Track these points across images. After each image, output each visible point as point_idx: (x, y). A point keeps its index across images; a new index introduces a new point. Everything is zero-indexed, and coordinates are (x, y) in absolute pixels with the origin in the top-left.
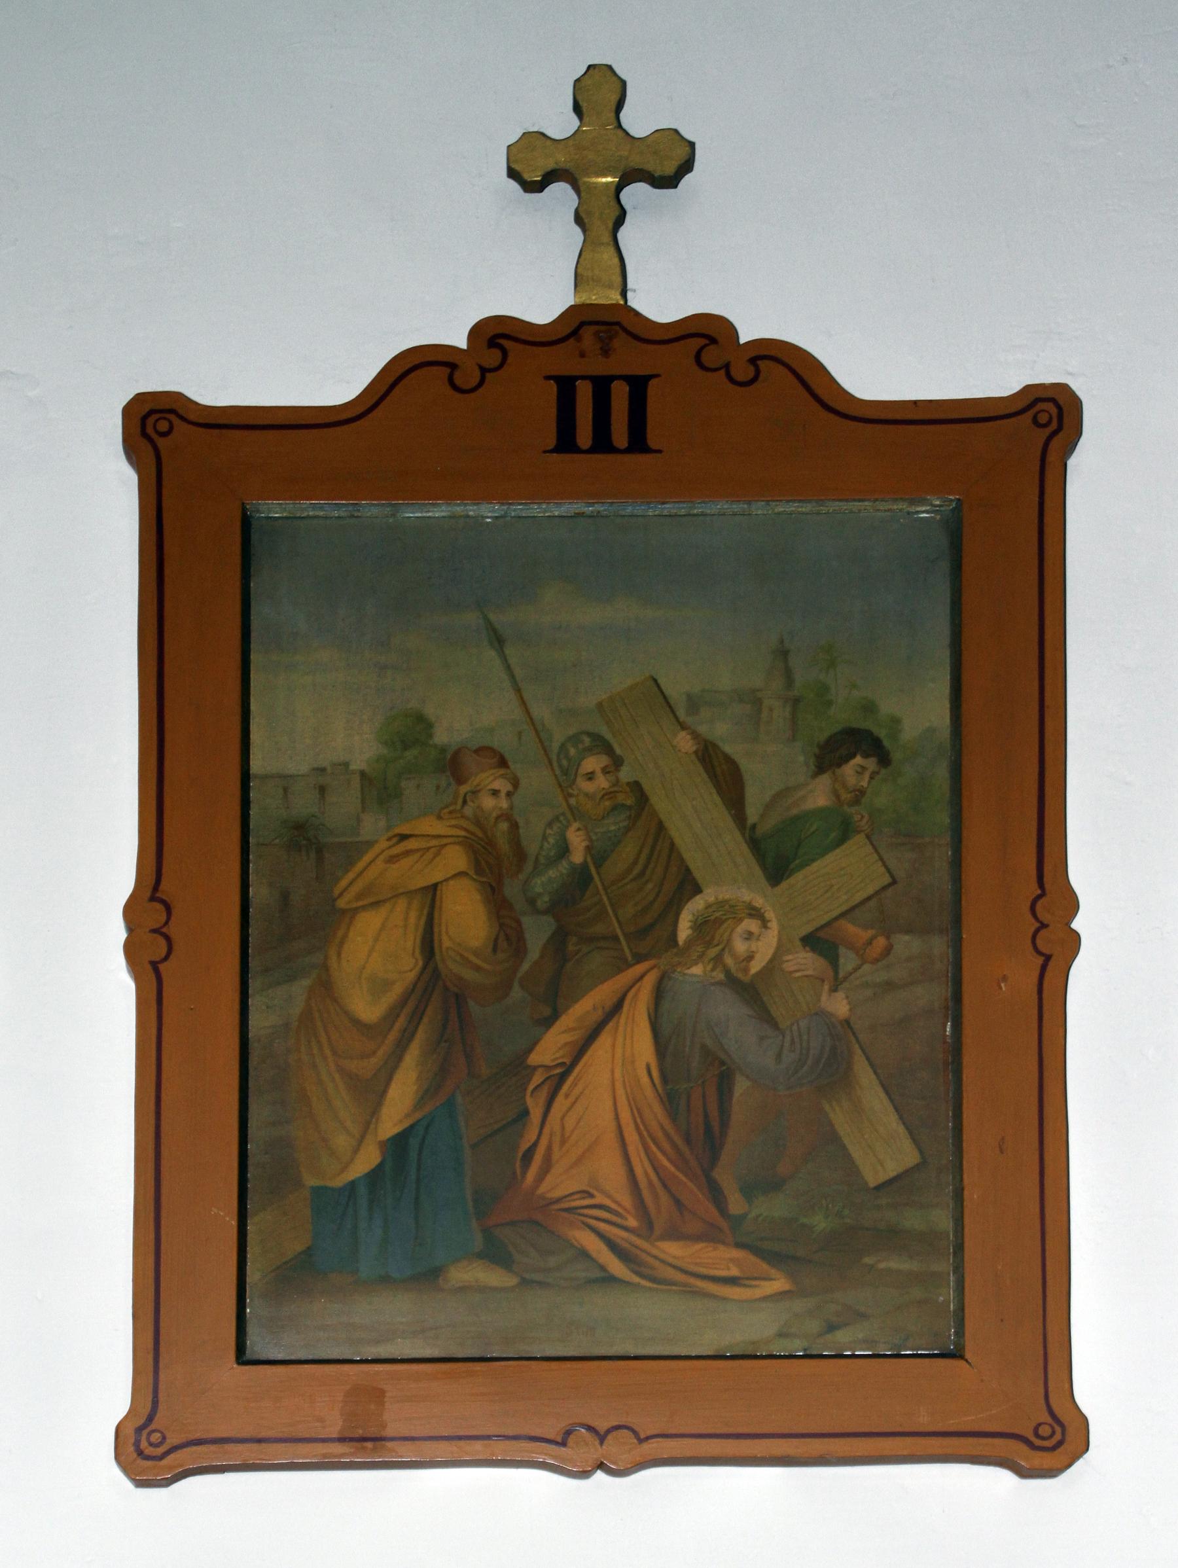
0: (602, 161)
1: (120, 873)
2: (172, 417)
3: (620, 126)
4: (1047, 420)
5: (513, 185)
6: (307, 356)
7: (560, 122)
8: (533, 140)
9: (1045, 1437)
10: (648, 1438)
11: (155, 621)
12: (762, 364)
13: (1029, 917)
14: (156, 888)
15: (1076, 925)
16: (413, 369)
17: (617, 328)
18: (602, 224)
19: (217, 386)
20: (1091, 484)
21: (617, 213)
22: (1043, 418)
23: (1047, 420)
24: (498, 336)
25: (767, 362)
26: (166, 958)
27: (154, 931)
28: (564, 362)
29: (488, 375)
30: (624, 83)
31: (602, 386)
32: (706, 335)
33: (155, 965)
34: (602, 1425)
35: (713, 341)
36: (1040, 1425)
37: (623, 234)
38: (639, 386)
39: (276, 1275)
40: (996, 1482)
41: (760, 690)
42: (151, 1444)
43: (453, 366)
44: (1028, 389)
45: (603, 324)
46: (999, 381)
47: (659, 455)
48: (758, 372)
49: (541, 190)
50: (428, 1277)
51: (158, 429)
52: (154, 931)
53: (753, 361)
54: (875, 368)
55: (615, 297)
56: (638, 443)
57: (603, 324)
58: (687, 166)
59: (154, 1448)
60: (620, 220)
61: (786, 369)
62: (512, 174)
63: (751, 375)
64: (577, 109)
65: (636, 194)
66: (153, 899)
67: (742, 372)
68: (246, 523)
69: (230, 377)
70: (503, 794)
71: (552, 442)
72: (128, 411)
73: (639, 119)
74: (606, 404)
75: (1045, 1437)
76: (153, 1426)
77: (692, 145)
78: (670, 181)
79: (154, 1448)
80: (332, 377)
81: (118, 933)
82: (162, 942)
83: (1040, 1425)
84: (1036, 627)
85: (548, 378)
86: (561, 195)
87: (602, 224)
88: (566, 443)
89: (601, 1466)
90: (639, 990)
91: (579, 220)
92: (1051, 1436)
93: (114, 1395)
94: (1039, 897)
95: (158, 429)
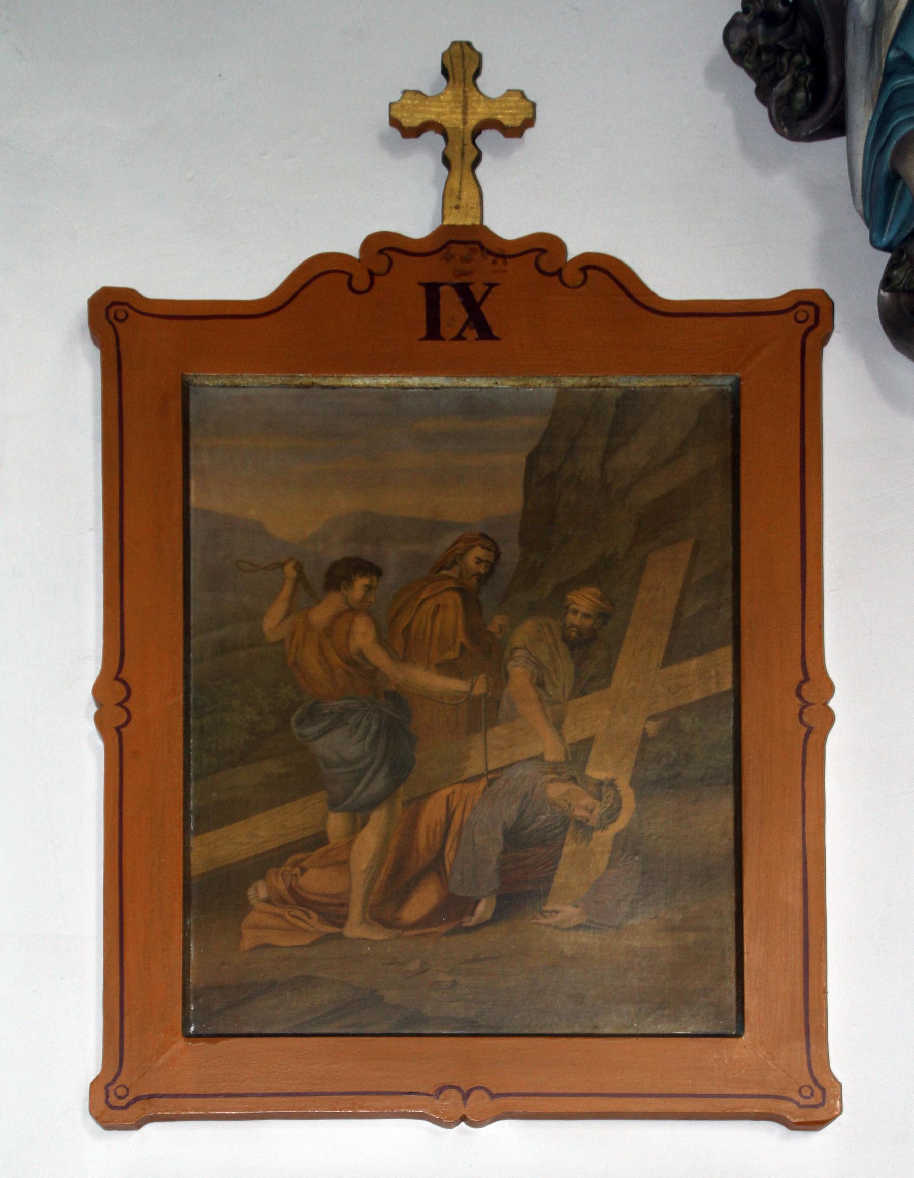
5: (397, 133)
6: (237, 262)
7: (426, 76)
9: (809, 1103)
12: (590, 272)
14: (119, 672)
17: (477, 246)
18: (461, 159)
19: (161, 283)
21: (475, 154)
22: (801, 316)
24: (384, 248)
25: (597, 272)
28: (435, 270)
32: (543, 249)
33: (118, 729)
35: (543, 251)
37: (479, 171)
39: (200, 995)
40: (767, 1135)
41: (552, 781)
45: (463, 245)
51: (115, 317)
53: (584, 269)
55: (478, 223)
58: (529, 123)
59: (121, 1101)
60: (477, 161)
61: (607, 276)
62: (395, 123)
64: (445, 72)
65: (488, 140)
66: (116, 679)
67: (572, 276)
68: (186, 389)
69: (176, 275)
71: (423, 333)
74: (452, 290)
75: (809, 1103)
76: (118, 1082)
78: (515, 132)
79: (121, 1101)
80: (251, 275)
85: (420, 284)
86: (433, 139)
87: (461, 159)
88: (433, 331)
89: (463, 1118)
91: (446, 161)
94: (803, 682)
95: (115, 317)
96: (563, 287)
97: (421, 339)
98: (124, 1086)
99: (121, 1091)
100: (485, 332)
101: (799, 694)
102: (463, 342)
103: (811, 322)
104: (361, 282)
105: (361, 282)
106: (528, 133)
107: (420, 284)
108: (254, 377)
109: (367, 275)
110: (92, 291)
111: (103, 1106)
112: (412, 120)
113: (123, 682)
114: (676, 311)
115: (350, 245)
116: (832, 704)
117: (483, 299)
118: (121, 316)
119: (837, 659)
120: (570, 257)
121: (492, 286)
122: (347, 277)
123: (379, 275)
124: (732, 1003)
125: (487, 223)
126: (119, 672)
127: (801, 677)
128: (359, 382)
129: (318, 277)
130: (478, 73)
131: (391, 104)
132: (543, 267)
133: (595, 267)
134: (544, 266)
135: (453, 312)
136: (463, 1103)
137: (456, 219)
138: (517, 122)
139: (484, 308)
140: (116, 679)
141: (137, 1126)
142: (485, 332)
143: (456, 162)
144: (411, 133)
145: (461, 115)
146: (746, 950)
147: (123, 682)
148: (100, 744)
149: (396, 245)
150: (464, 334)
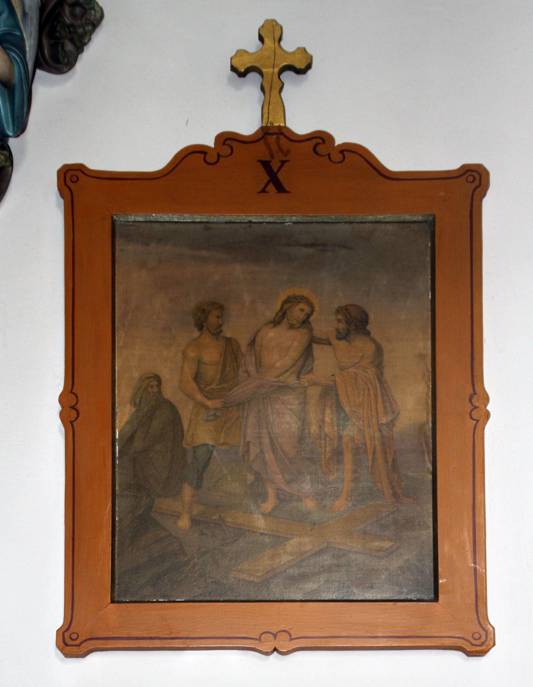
0: (271, 65)
1: (55, 380)
2: (78, 173)
4: (473, 180)
5: (235, 75)
7: (252, 44)
8: (241, 53)
9: (477, 643)
11: (71, 265)
13: (470, 405)
14: (476, 424)
15: (488, 408)
16: (191, 155)
18: (272, 91)
19: (96, 163)
20: (493, 209)
21: (281, 84)
23: (473, 180)
24: (227, 140)
26: (471, 411)
29: (74, 423)
30: (281, 28)
32: (320, 139)
33: (71, 422)
34: (274, 630)
37: (283, 94)
42: (71, 176)
43: (205, 153)
44: (463, 166)
46: (450, 163)
53: (342, 152)
57: (273, 135)
58: (309, 67)
59: (73, 642)
61: (357, 158)
62: (233, 69)
65: (287, 76)
68: (113, 223)
70: (305, 312)
72: (59, 172)
73: (289, 44)
75: (477, 643)
77: (311, 58)
78: (302, 71)
79: (73, 642)
80: (150, 156)
81: (58, 407)
82: (216, 159)
86: (253, 76)
87: (272, 91)
89: (275, 650)
90: (427, 444)
91: (262, 89)
92: (479, 639)
93: (57, 618)
96: (316, 156)
99: (74, 636)
100: (280, 188)
101: (470, 401)
102: (265, 194)
104: (212, 159)
106: (310, 72)
109: (216, 155)
110: (59, 166)
113: (74, 394)
115: (209, 141)
116: (488, 408)
118: (75, 179)
119: (491, 380)
123: (222, 157)
124: (434, 590)
125: (287, 125)
126: (476, 424)
127: (472, 392)
128: (166, 217)
129: (190, 157)
130: (280, 39)
131: (231, 59)
132: (209, 161)
133: (347, 151)
136: (274, 643)
138: (301, 68)
139: (280, 176)
141: (84, 655)
142: (280, 188)
143: (267, 89)
144: (242, 75)
145: (271, 65)
147: (74, 394)
148: (63, 429)
150: (266, 190)
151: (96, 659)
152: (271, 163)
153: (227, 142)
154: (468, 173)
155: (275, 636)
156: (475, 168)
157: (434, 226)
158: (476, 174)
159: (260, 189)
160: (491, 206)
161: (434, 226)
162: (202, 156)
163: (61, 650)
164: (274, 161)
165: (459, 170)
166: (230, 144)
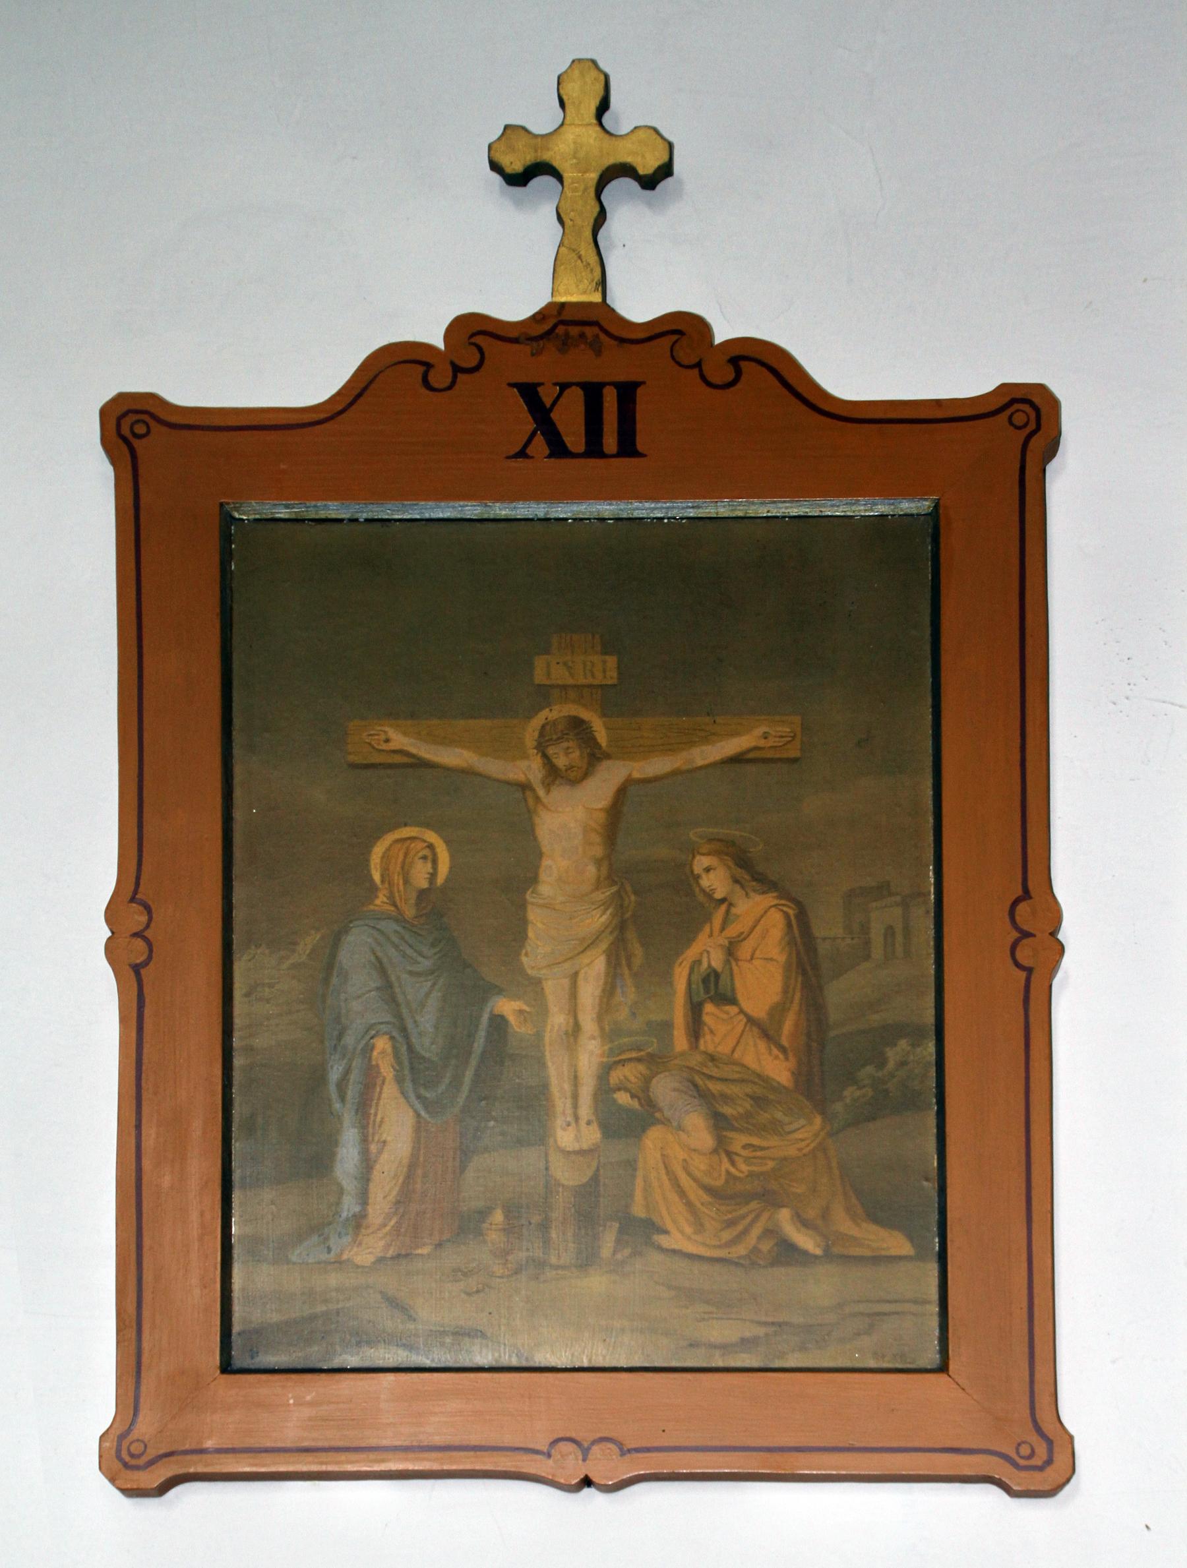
0: (579, 164)
1: (100, 872)
3: (536, 136)
4: (1023, 423)
5: (496, 178)
6: (284, 358)
9: (1032, 1457)
10: (629, 1451)
18: (587, 234)
19: (187, 390)
20: (1075, 496)
22: (1019, 419)
23: (1023, 423)
24: (473, 331)
27: (136, 935)
31: (592, 392)
32: (681, 331)
33: (137, 969)
34: (585, 1436)
36: (1024, 1442)
38: (628, 392)
39: (206, 1381)
40: (984, 1500)
43: (428, 366)
44: (1003, 387)
46: (966, 380)
47: (512, 381)
48: (739, 373)
49: (524, 184)
50: (377, 1066)
51: (136, 429)
52: (136, 935)
53: (735, 361)
54: (853, 368)
55: (596, 298)
56: (628, 448)
57: (580, 327)
59: (142, 1463)
60: (601, 217)
61: (764, 368)
62: (495, 166)
63: (731, 376)
66: (1029, 970)
72: (104, 412)
78: (650, 182)
79: (142, 1463)
80: (306, 377)
81: (1067, 934)
83: (1024, 1442)
84: (1017, 632)
85: (511, 385)
87: (587, 234)
93: (100, 1407)
95: (136, 429)
97: (508, 458)
98: (143, 1441)
99: (136, 1448)
103: (1032, 426)
104: (440, 377)
105: (440, 377)
107: (511, 385)
108: (287, 507)
111: (117, 1465)
112: (515, 165)
114: (969, 412)
117: (534, 434)
118: (140, 429)
120: (441, 345)
121: (522, 454)
122: (421, 369)
129: (393, 371)
130: (604, 106)
131: (490, 147)
134: (681, 355)
135: (570, 418)
137: (577, 293)
139: (555, 416)
140: (133, 899)
144: (518, 179)
146: (219, 1221)
149: (490, 329)
151: (192, 1499)
152: (540, 389)
153: (479, 340)
154: (1016, 406)
155: (698, 365)
156: (1060, 1459)
157: (907, 563)
158: (1026, 408)
159: (517, 450)
160: (1067, 488)
161: (907, 563)
162: (421, 369)
163: (112, 1480)
164: (582, 384)
165: (114, 461)
166: (482, 344)
